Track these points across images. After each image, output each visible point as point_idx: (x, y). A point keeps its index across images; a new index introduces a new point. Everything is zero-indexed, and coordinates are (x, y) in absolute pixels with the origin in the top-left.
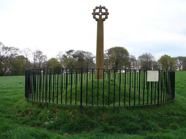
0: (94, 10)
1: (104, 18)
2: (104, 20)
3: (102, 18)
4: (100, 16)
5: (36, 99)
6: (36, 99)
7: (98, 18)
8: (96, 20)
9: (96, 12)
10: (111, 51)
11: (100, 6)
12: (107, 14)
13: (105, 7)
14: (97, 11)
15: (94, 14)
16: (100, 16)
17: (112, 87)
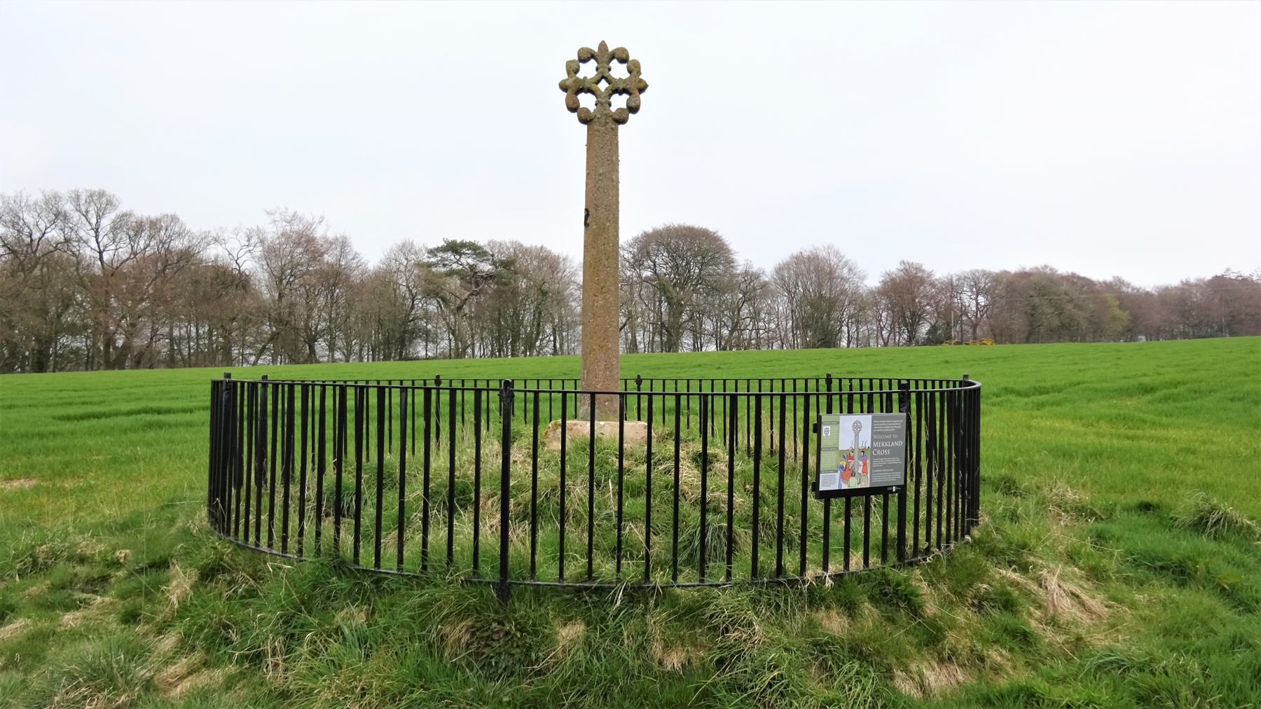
0: (572, 69)
1: (620, 110)
2: (623, 121)
3: (613, 109)
4: (603, 103)
5: (241, 533)
6: (241, 533)
7: (592, 108)
8: (583, 121)
9: (580, 75)
10: (650, 243)
11: (603, 46)
12: (634, 88)
13: (624, 50)
14: (588, 71)
15: (572, 88)
16: (603, 103)
17: (691, 514)
